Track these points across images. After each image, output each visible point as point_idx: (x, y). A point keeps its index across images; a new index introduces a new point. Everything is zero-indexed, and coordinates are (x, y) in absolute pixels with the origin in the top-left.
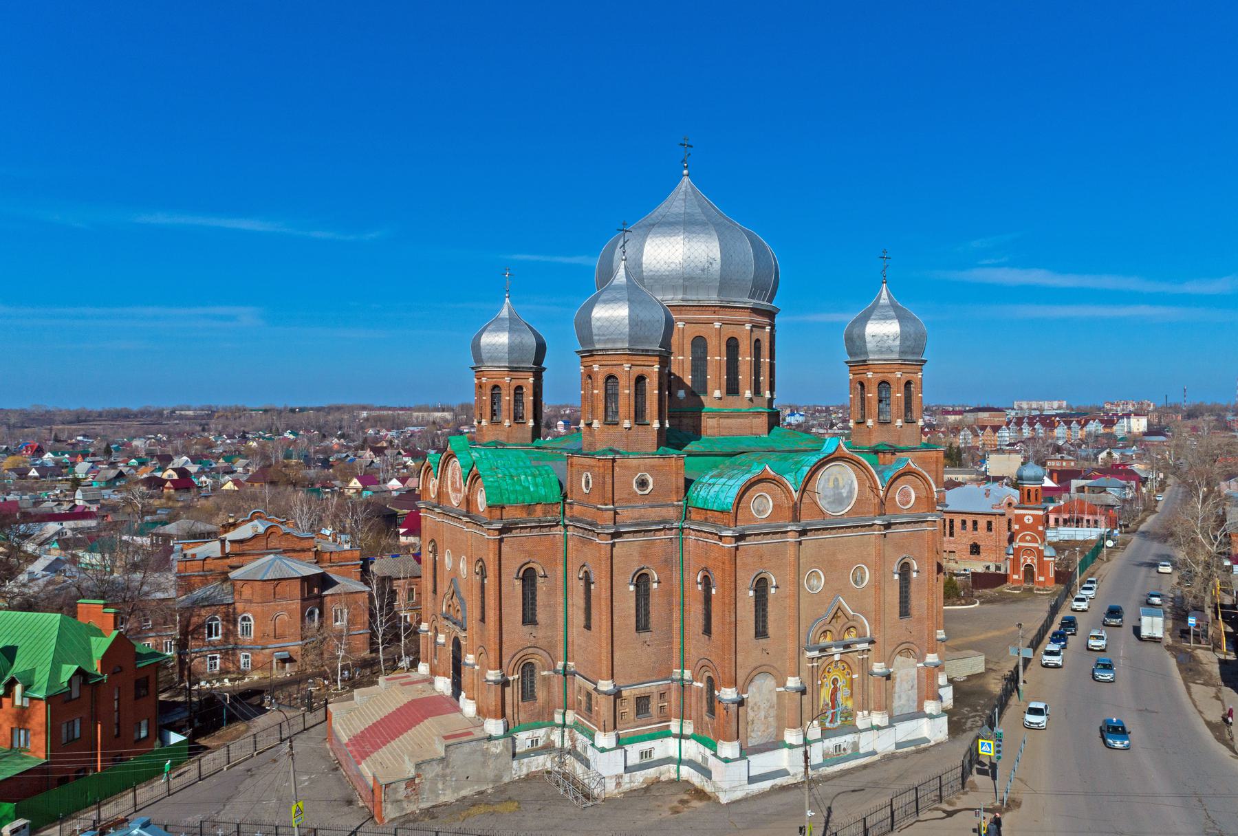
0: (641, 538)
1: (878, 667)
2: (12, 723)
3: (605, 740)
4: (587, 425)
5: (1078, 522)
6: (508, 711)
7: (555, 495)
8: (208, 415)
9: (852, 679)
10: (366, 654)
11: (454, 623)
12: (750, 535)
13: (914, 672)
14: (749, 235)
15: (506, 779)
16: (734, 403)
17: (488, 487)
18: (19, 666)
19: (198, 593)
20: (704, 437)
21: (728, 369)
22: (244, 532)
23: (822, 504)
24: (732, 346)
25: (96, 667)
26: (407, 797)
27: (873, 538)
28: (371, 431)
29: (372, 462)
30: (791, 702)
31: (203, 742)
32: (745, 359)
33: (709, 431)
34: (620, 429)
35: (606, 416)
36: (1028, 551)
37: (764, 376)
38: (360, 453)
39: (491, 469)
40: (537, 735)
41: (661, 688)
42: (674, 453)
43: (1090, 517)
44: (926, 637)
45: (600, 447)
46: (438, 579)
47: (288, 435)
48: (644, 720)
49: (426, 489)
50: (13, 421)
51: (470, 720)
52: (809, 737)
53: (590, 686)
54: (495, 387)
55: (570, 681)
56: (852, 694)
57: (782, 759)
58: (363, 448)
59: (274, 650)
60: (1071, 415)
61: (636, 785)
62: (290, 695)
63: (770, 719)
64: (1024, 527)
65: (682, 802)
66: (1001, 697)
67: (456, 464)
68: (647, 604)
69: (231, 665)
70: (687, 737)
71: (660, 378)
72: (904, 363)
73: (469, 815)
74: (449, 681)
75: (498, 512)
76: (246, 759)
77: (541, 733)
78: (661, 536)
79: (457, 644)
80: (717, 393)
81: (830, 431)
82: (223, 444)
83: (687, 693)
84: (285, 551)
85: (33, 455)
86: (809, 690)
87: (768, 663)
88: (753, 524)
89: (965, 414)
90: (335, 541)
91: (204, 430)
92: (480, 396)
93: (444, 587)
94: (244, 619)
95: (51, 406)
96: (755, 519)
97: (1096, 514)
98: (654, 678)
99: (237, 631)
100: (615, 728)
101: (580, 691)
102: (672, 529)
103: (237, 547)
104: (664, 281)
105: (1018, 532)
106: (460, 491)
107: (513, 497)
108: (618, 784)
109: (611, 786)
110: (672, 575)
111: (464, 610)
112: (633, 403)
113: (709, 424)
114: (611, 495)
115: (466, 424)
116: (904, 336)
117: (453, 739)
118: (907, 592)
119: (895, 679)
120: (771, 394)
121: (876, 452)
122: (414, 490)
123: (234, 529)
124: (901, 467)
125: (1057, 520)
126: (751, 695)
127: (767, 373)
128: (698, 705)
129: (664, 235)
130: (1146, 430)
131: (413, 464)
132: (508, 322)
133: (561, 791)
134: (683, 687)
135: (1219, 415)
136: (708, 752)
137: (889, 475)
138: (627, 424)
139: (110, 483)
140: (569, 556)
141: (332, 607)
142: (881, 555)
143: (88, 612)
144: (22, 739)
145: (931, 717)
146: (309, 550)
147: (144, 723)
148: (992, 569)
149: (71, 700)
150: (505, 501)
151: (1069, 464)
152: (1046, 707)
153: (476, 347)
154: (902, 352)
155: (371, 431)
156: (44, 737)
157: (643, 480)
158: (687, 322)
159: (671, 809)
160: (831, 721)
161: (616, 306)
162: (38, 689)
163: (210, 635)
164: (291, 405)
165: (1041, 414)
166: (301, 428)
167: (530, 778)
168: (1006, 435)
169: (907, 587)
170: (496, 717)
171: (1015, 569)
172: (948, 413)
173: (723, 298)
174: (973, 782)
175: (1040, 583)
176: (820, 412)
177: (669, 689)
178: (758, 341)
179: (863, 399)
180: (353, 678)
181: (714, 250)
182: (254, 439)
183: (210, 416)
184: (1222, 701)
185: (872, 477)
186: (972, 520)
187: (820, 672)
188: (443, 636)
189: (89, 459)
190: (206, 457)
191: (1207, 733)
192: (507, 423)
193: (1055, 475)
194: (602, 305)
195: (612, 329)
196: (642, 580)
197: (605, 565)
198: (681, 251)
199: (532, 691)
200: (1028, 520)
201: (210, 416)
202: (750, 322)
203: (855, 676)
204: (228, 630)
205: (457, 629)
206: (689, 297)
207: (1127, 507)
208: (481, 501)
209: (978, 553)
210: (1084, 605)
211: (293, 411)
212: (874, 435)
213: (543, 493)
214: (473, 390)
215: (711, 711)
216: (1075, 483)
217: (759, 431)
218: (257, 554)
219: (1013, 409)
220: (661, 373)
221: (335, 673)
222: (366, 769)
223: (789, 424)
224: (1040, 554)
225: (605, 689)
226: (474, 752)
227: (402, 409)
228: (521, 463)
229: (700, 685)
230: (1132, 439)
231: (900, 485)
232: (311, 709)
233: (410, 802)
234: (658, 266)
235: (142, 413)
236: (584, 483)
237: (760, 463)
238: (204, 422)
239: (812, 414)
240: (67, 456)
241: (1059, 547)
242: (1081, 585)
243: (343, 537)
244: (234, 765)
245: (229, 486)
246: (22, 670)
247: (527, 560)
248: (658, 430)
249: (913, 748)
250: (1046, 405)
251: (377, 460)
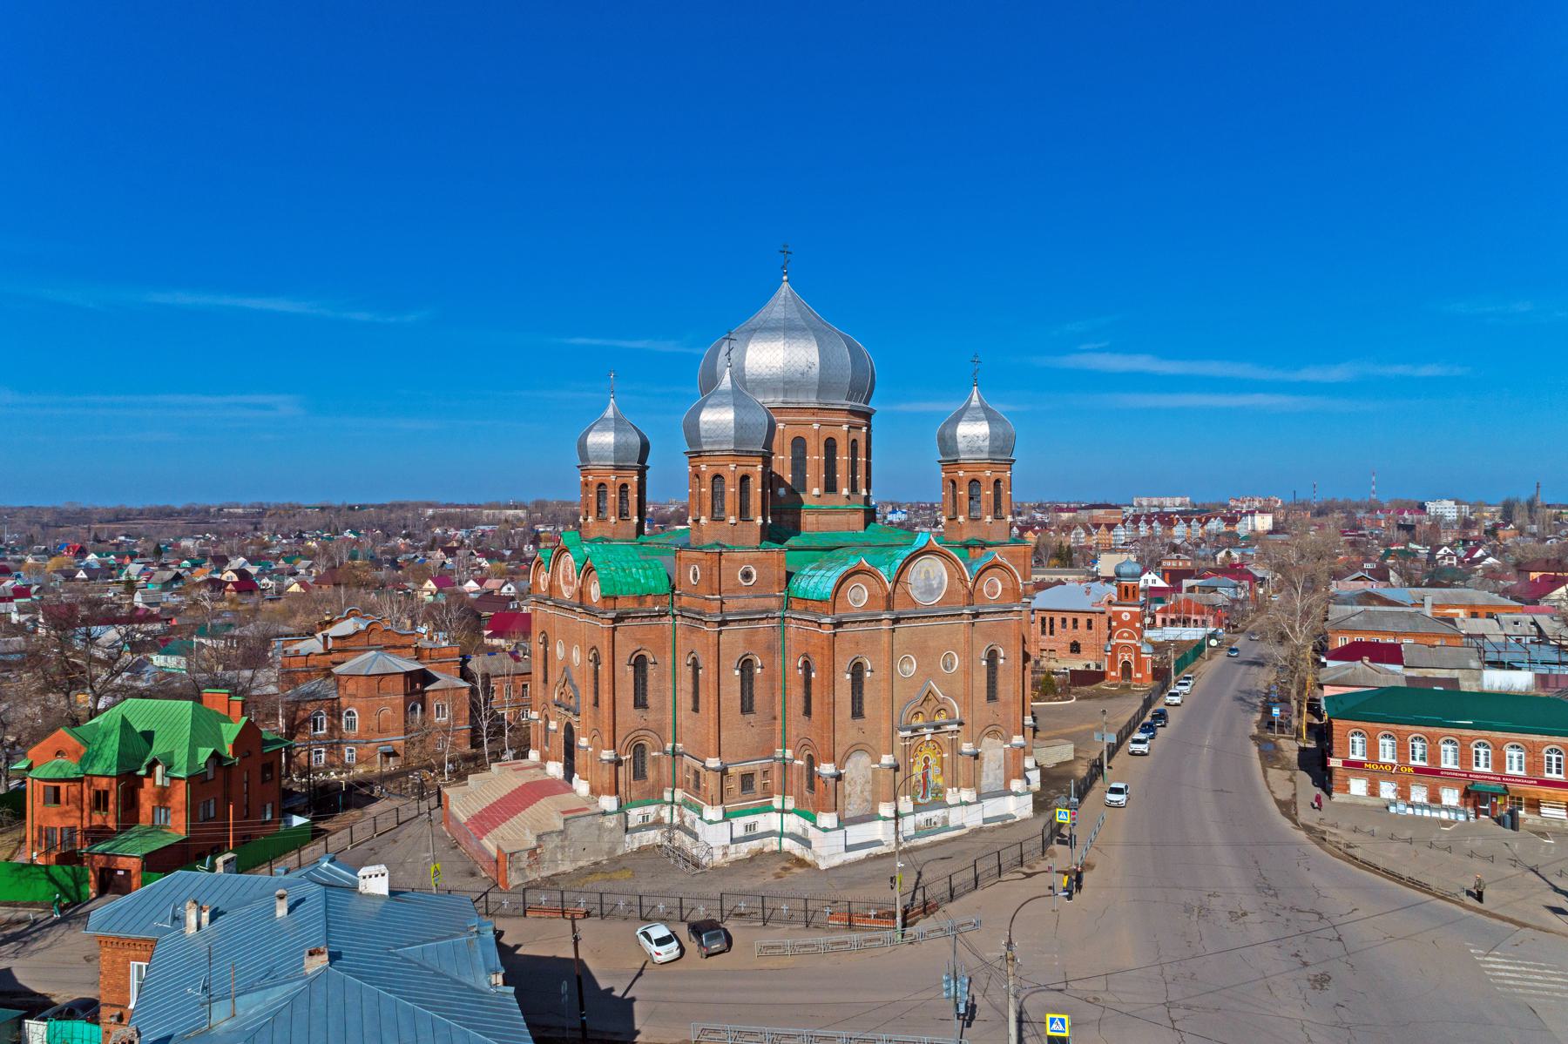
0: (745, 626)
1: (967, 747)
2: (153, 802)
3: (712, 813)
4: (694, 521)
5: (1186, 622)
6: (621, 788)
7: (664, 587)
8: (259, 513)
9: (942, 758)
10: (467, 749)
11: (567, 710)
12: (847, 623)
13: (1001, 752)
14: (846, 339)
15: (620, 852)
16: (832, 501)
17: (602, 579)
18: (158, 749)
19: (304, 688)
20: (803, 533)
21: (826, 467)
22: (346, 627)
23: (914, 594)
24: (830, 446)
25: (228, 750)
26: (529, 866)
27: (962, 627)
28: (438, 531)
29: (444, 563)
30: (885, 779)
31: (321, 826)
32: (843, 458)
33: (808, 528)
34: (726, 525)
35: (713, 512)
36: (1126, 648)
38: (430, 553)
39: (604, 562)
41: (764, 766)
42: (776, 547)
43: (1198, 617)
44: (1012, 720)
45: (707, 541)
46: (549, 669)
47: (348, 534)
48: (749, 796)
49: (536, 583)
50: (45, 519)
51: (583, 798)
52: (902, 810)
53: (698, 765)
54: (601, 485)
55: (678, 761)
56: (942, 773)
57: (878, 831)
58: (432, 549)
59: (375, 747)
60: (1193, 513)
61: (741, 855)
62: (401, 785)
63: (866, 794)
64: (1122, 624)
65: (785, 869)
66: (1085, 779)
67: (568, 560)
68: (751, 688)
69: (336, 759)
70: (789, 812)
71: (763, 477)
72: (993, 463)
73: (587, 882)
74: (561, 765)
76: (367, 840)
78: (764, 624)
79: (569, 730)
80: (816, 491)
81: (934, 530)
82: (279, 544)
83: (788, 771)
84: (386, 648)
85: (76, 556)
86: (902, 767)
88: (849, 612)
89: (1079, 511)
90: (431, 638)
91: (256, 529)
92: (586, 494)
93: (555, 675)
94: (349, 714)
95: (86, 502)
96: (852, 608)
97: (1203, 613)
98: (758, 757)
99: (341, 725)
100: (722, 802)
101: (688, 771)
102: (774, 618)
103: (339, 643)
104: (765, 384)
105: (1117, 628)
106: (572, 584)
107: (625, 588)
108: (725, 854)
109: (718, 855)
110: (774, 661)
111: (577, 696)
112: (738, 500)
113: (808, 520)
114: (717, 586)
115: (541, 523)
116: (993, 437)
117: (571, 815)
118: (994, 678)
119: (983, 759)
120: (868, 491)
121: (967, 547)
122: (493, 592)
123: (331, 627)
124: (987, 561)
125: (1164, 621)
126: (849, 770)
127: (864, 472)
128: (798, 782)
129: (765, 340)
130: (1271, 528)
131: (488, 565)
132: (613, 422)
133: (672, 861)
134: (785, 765)
135: (1350, 512)
136: (808, 824)
137: (977, 567)
138: (732, 520)
139: (166, 586)
140: (677, 644)
141: (433, 702)
142: (970, 643)
143: (214, 701)
144: (163, 816)
145: (1016, 794)
146: (410, 647)
147: (269, 806)
148: (1093, 668)
149: (207, 781)
150: (618, 593)
151: (1184, 563)
152: (1126, 787)
153: (582, 446)
154: (990, 452)
155: (438, 531)
156: (184, 814)
158: (787, 423)
159: (775, 874)
160: (922, 797)
161: (722, 410)
162: (179, 769)
163: (315, 730)
164: (350, 502)
165: (1161, 512)
166: (362, 527)
167: (641, 851)
168: (1121, 534)
169: (994, 673)
170: (610, 794)
171: (1113, 666)
172: (1062, 510)
173: (821, 401)
174: (1053, 850)
175: (1137, 679)
176: (924, 509)
177: (772, 767)
178: (854, 441)
179: (954, 496)
180: (459, 770)
181: (813, 354)
182: (311, 540)
183: (261, 515)
184: (1295, 783)
185: (961, 569)
186: (1072, 618)
187: (912, 751)
188: (555, 723)
189: (137, 560)
190: (264, 558)
191: (1274, 807)
192: (613, 519)
193: (1167, 575)
194: (710, 409)
195: (719, 432)
196: (746, 666)
197: (712, 650)
198: (781, 355)
199: (643, 771)
200: (1126, 617)
201: (261, 515)
202: (847, 423)
203: (945, 755)
204: (333, 724)
205: (570, 714)
206: (789, 400)
207: (1238, 607)
208: (595, 592)
209: (1079, 652)
210: (1177, 700)
211: (351, 508)
212: (965, 531)
213: (653, 584)
214: (579, 487)
215: (811, 787)
216: (1186, 583)
217: (856, 527)
218: (359, 651)
219: (1132, 506)
220: (764, 473)
221: (442, 766)
222: (489, 844)
223: (891, 523)
224: (1138, 651)
225: (713, 766)
226: (589, 826)
227: (470, 506)
228: (630, 558)
229: (800, 762)
230: (1254, 538)
231: (987, 578)
232: (422, 798)
233: (532, 870)
234: (760, 370)
235: (187, 511)
236: (692, 575)
237: (856, 555)
238: (254, 520)
239: (915, 512)
240: (112, 557)
241: (1158, 647)
242: (1176, 682)
243: (441, 634)
244: (357, 845)
245: (295, 588)
246: (161, 752)
247: (639, 648)
249: (1000, 823)
250: (1167, 501)
251: (449, 561)
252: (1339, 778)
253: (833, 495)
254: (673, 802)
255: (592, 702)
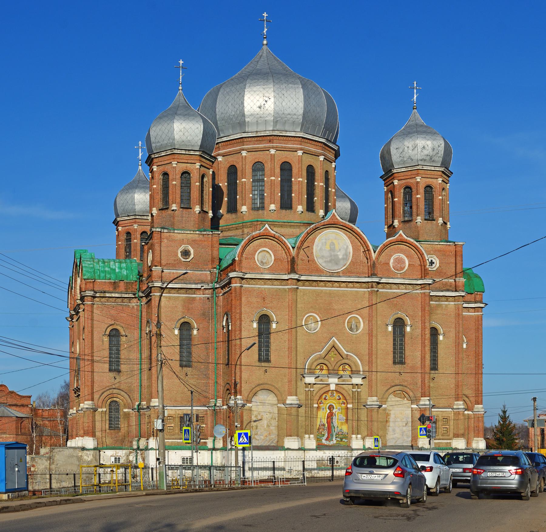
9: (347, 408)
13: (409, 412)
16: (286, 216)
24: (311, 171)
32: (319, 184)
37: (399, 197)
40: (119, 455)
56: (347, 420)
63: (272, 428)
75: (248, 399)
77: (121, 453)
87: (269, 383)
157: (186, 250)
160: (327, 439)
213: (125, 273)
247: (113, 322)
248: (211, 219)
252: (263, 465)
253: (288, 211)
254: (138, 448)
255: (222, 360)
